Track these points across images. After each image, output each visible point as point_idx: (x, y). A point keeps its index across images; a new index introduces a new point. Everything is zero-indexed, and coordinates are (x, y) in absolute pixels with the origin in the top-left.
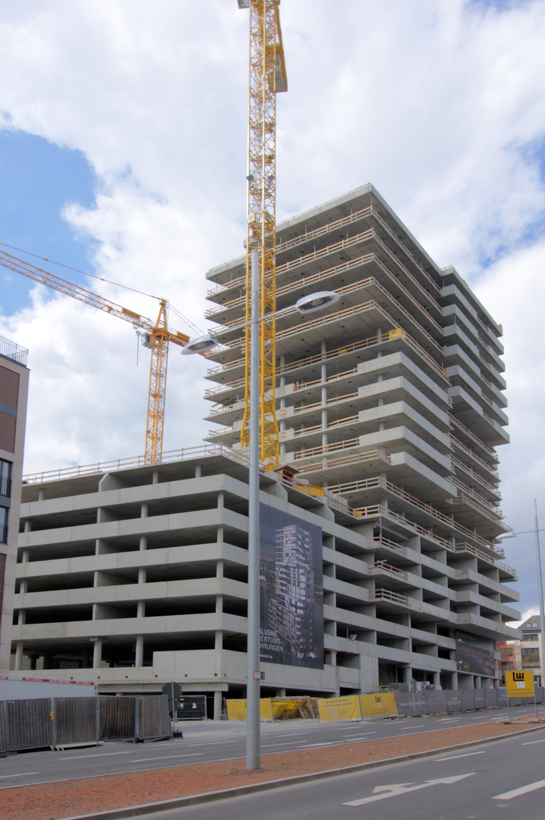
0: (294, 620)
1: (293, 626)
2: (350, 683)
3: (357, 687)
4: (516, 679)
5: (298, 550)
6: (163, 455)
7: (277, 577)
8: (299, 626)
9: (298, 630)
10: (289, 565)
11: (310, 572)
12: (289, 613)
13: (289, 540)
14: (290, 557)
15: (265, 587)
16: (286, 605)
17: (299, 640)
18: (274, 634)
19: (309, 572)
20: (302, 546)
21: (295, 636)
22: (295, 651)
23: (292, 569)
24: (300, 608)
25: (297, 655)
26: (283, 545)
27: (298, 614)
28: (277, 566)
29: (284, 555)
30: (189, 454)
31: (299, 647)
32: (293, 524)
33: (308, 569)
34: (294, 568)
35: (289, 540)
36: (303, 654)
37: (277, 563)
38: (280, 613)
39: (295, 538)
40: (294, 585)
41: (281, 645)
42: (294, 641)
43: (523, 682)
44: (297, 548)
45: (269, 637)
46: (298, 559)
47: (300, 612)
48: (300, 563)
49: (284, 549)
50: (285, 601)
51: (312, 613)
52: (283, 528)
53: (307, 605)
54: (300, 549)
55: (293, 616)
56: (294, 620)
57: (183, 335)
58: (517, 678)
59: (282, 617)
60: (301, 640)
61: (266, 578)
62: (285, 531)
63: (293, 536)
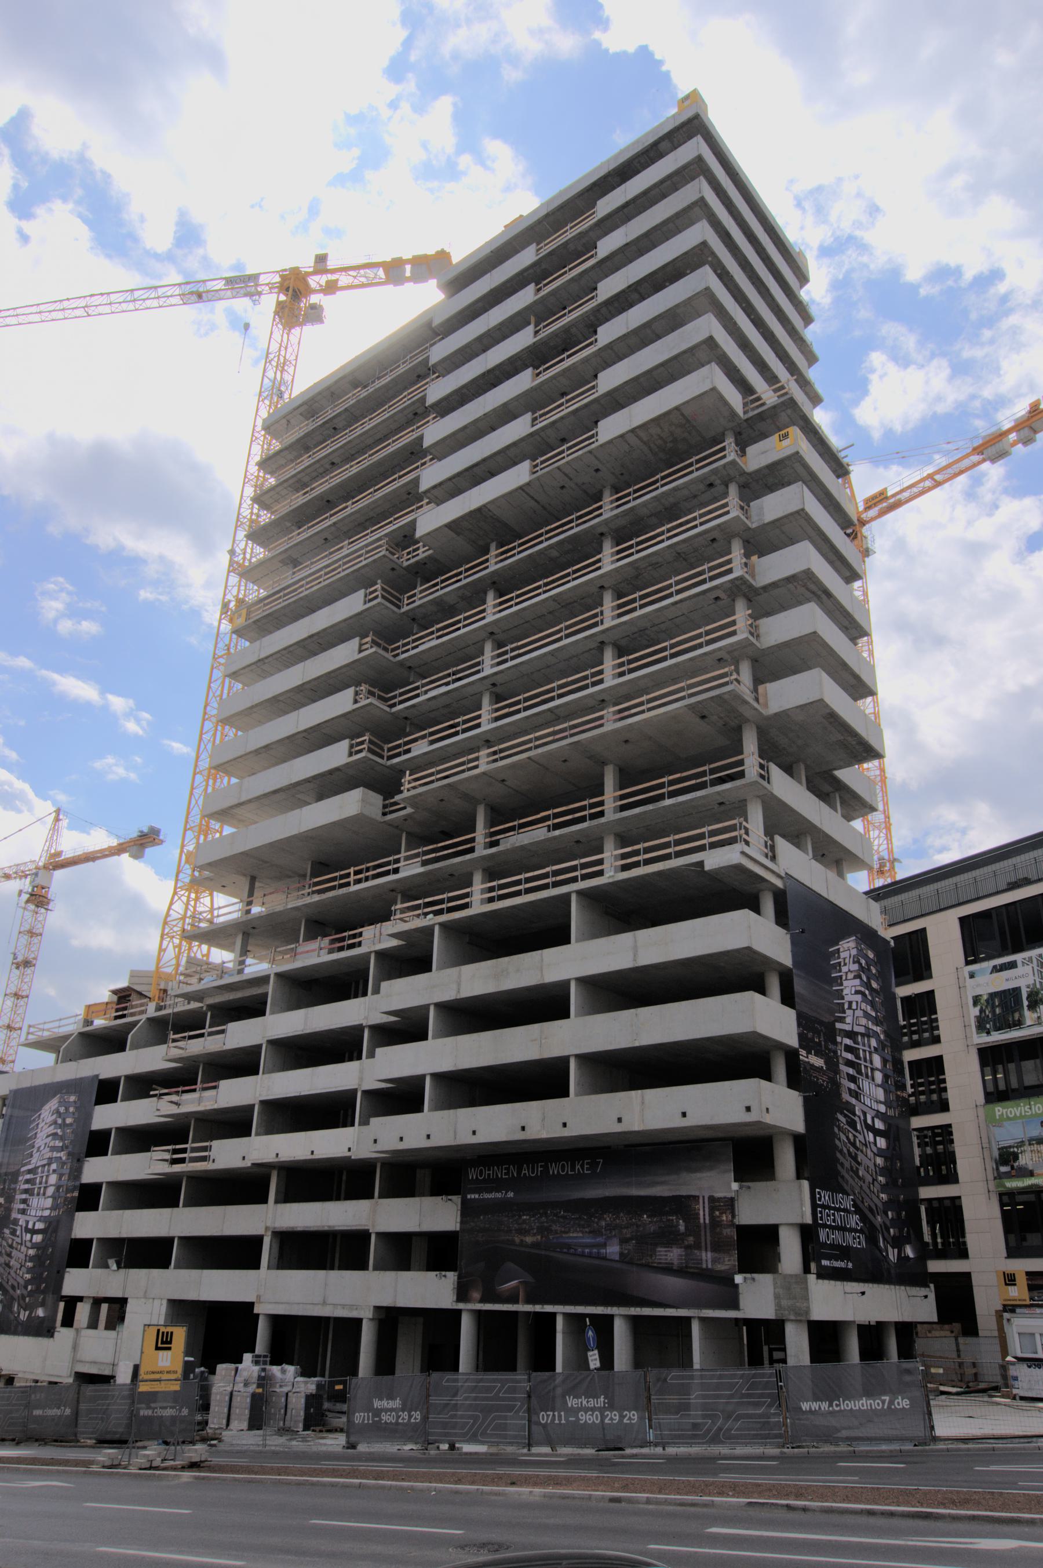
0: (875, 1164)
1: (874, 1180)
2: (95, 1363)
3: (107, 1372)
4: (160, 1345)
5: (863, 994)
6: (216, 913)
7: (841, 1061)
8: (30, 1264)
9: (884, 1188)
10: (856, 1029)
11: (885, 1045)
12: (864, 1148)
13: (849, 971)
14: (854, 1010)
15: (825, 1084)
16: (859, 1127)
17: (887, 1215)
18: (847, 1203)
19: (64, 1163)
20: (868, 985)
21: (22, 1282)
22: (18, 1309)
23: (860, 1037)
24: (38, 1232)
25: (19, 1315)
26: (841, 984)
27: (879, 1149)
28: (838, 1032)
29: (846, 1006)
30: (230, 913)
31: (25, 1300)
32: (850, 936)
33: (882, 1037)
34: (863, 1035)
35: (849, 971)
36: (27, 1313)
37: (838, 1025)
38: (852, 1149)
39: (856, 967)
40: (867, 1077)
41: (861, 1231)
42: (18, 1292)
43: (169, 1353)
44: (863, 989)
45: (842, 1213)
46: (866, 1015)
47: (882, 1143)
48: (870, 1025)
49: (845, 992)
50: (856, 1119)
51: (54, 1235)
52: (837, 944)
53: (50, 1223)
54: (867, 992)
55: (872, 1155)
56: (875, 1164)
57: (874, 497)
58: (163, 1343)
59: (855, 1158)
60: (29, 1288)
61: (826, 1063)
62: (841, 950)
63: (854, 962)
